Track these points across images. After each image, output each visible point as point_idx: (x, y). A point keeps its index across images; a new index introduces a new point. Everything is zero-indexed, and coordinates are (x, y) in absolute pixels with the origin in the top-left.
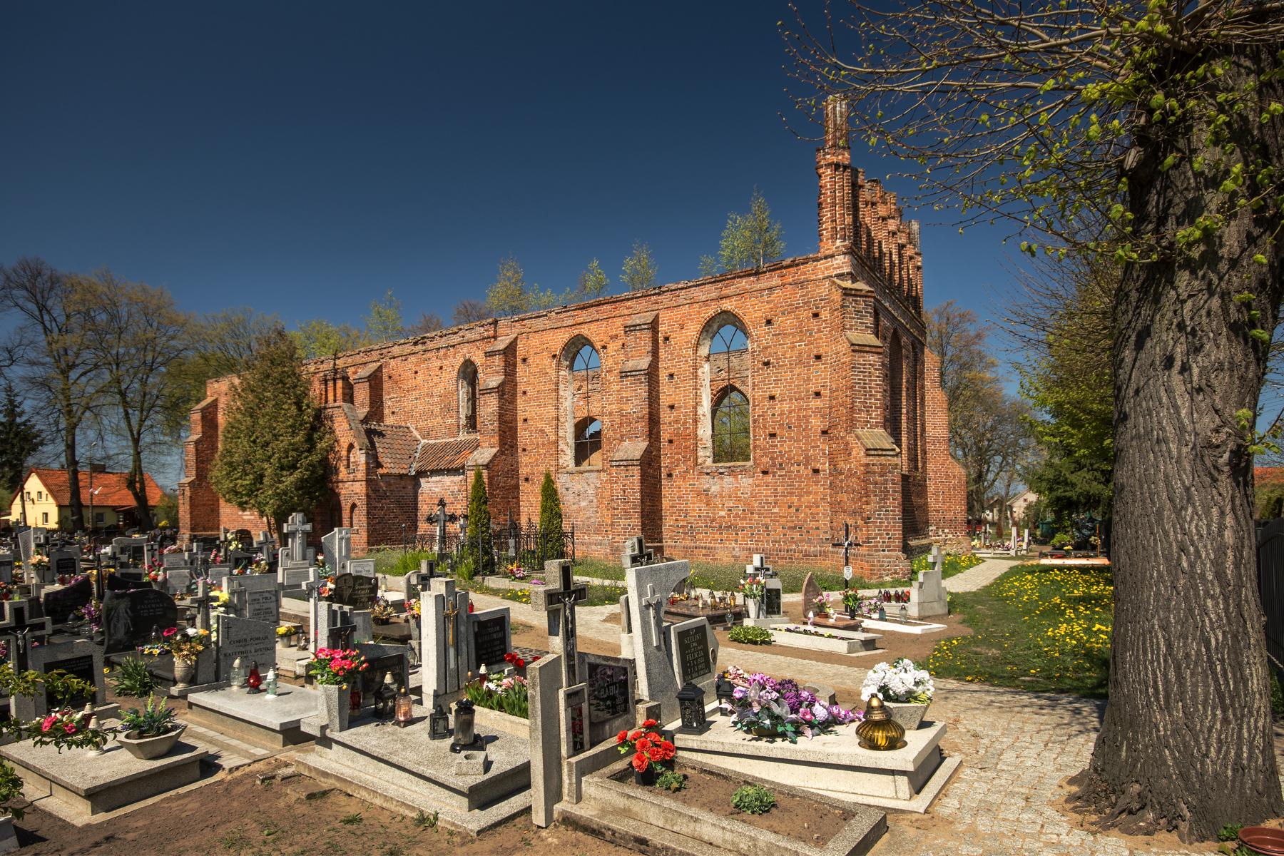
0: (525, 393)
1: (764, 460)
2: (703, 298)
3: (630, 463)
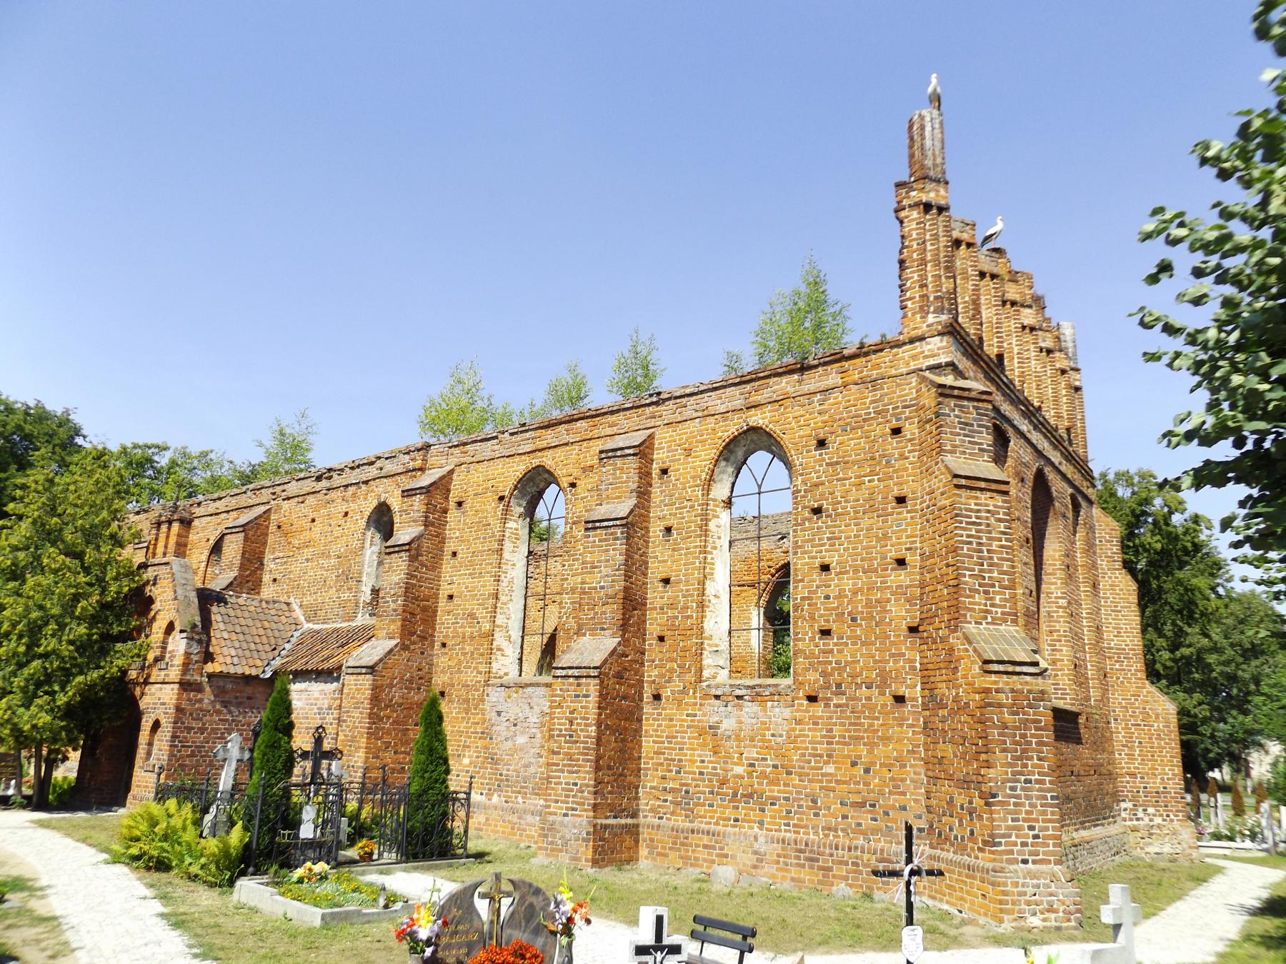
0: (454, 554)
1: (812, 676)
2: (722, 409)
3: (584, 672)
